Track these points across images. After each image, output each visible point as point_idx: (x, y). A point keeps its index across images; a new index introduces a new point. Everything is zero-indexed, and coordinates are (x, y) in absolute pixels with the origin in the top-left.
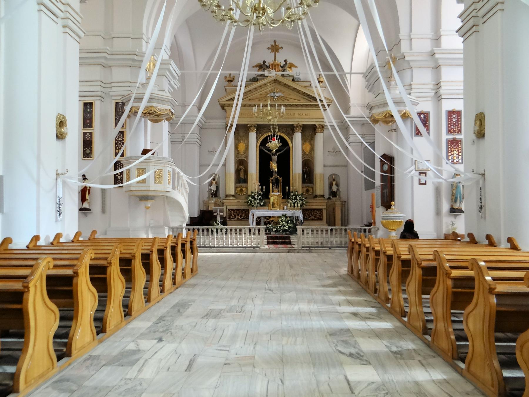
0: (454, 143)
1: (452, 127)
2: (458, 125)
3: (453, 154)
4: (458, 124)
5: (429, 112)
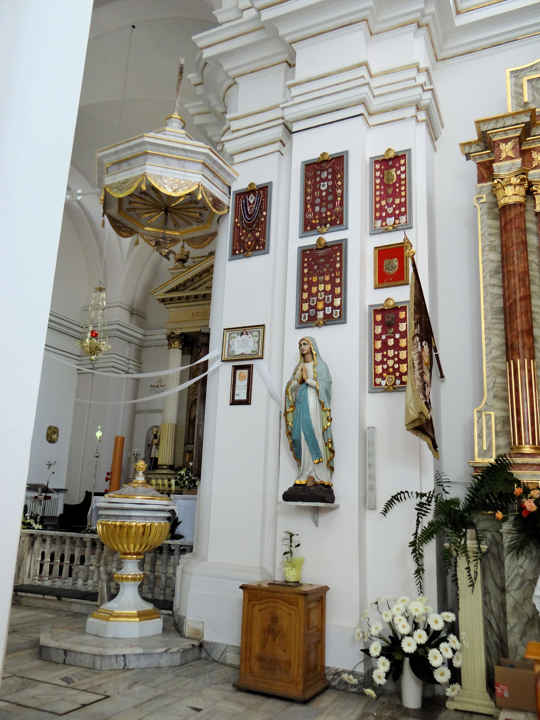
1: (317, 209)
3: (316, 295)
4: (336, 197)
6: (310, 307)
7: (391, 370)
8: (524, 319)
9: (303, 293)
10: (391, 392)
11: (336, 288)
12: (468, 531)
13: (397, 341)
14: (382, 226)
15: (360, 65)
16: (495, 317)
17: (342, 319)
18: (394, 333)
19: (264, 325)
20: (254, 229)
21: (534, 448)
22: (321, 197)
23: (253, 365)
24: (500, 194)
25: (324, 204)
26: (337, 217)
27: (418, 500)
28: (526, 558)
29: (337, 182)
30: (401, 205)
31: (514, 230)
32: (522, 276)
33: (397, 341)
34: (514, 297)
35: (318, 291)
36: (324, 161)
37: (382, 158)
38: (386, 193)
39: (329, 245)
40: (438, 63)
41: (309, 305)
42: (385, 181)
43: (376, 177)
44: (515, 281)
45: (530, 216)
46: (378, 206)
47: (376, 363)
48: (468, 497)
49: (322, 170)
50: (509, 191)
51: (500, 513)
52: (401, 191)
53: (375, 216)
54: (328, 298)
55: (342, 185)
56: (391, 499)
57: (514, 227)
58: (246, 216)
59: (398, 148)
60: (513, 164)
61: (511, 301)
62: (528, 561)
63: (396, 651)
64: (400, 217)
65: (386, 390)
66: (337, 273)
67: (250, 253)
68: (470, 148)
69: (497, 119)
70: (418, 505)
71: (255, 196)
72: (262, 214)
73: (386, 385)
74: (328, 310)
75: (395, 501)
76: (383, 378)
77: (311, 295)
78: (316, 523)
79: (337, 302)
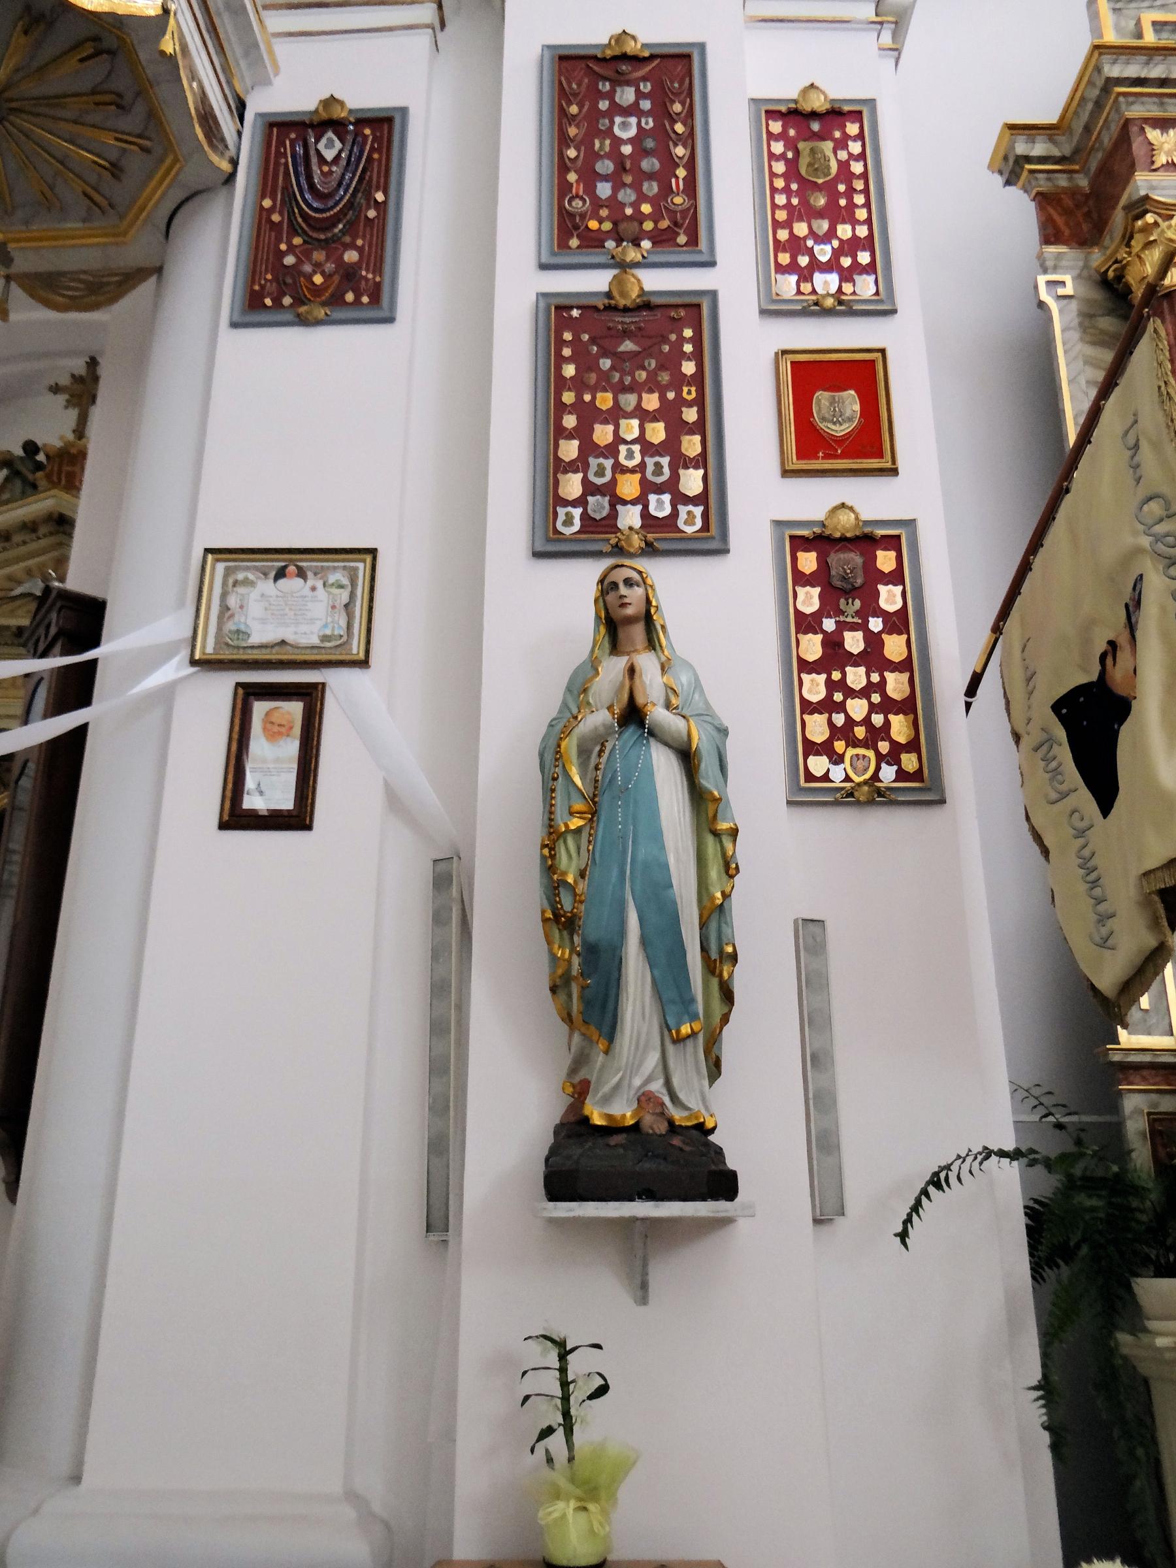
0: (626, 334)
1: (604, 190)
2: (664, 177)
3: (611, 450)
4: (671, 164)
5: (404, 111)
6: (589, 488)
7: (860, 732)
9: (562, 442)
13: (874, 642)
19: (373, 552)
20: (336, 239)
23: (324, 684)
29: (673, 121)
30: (852, 246)
33: (874, 642)
35: (618, 440)
36: (624, 57)
38: (804, 202)
41: (585, 482)
42: (803, 172)
46: (783, 235)
49: (620, 81)
52: (852, 206)
54: (658, 466)
55: (691, 133)
58: (308, 196)
64: (856, 277)
65: (848, 798)
66: (685, 389)
67: (321, 313)
68: (1030, 145)
71: (342, 140)
72: (369, 197)
73: (848, 779)
74: (661, 505)
76: (837, 759)
77: (589, 448)
78: (642, 1292)
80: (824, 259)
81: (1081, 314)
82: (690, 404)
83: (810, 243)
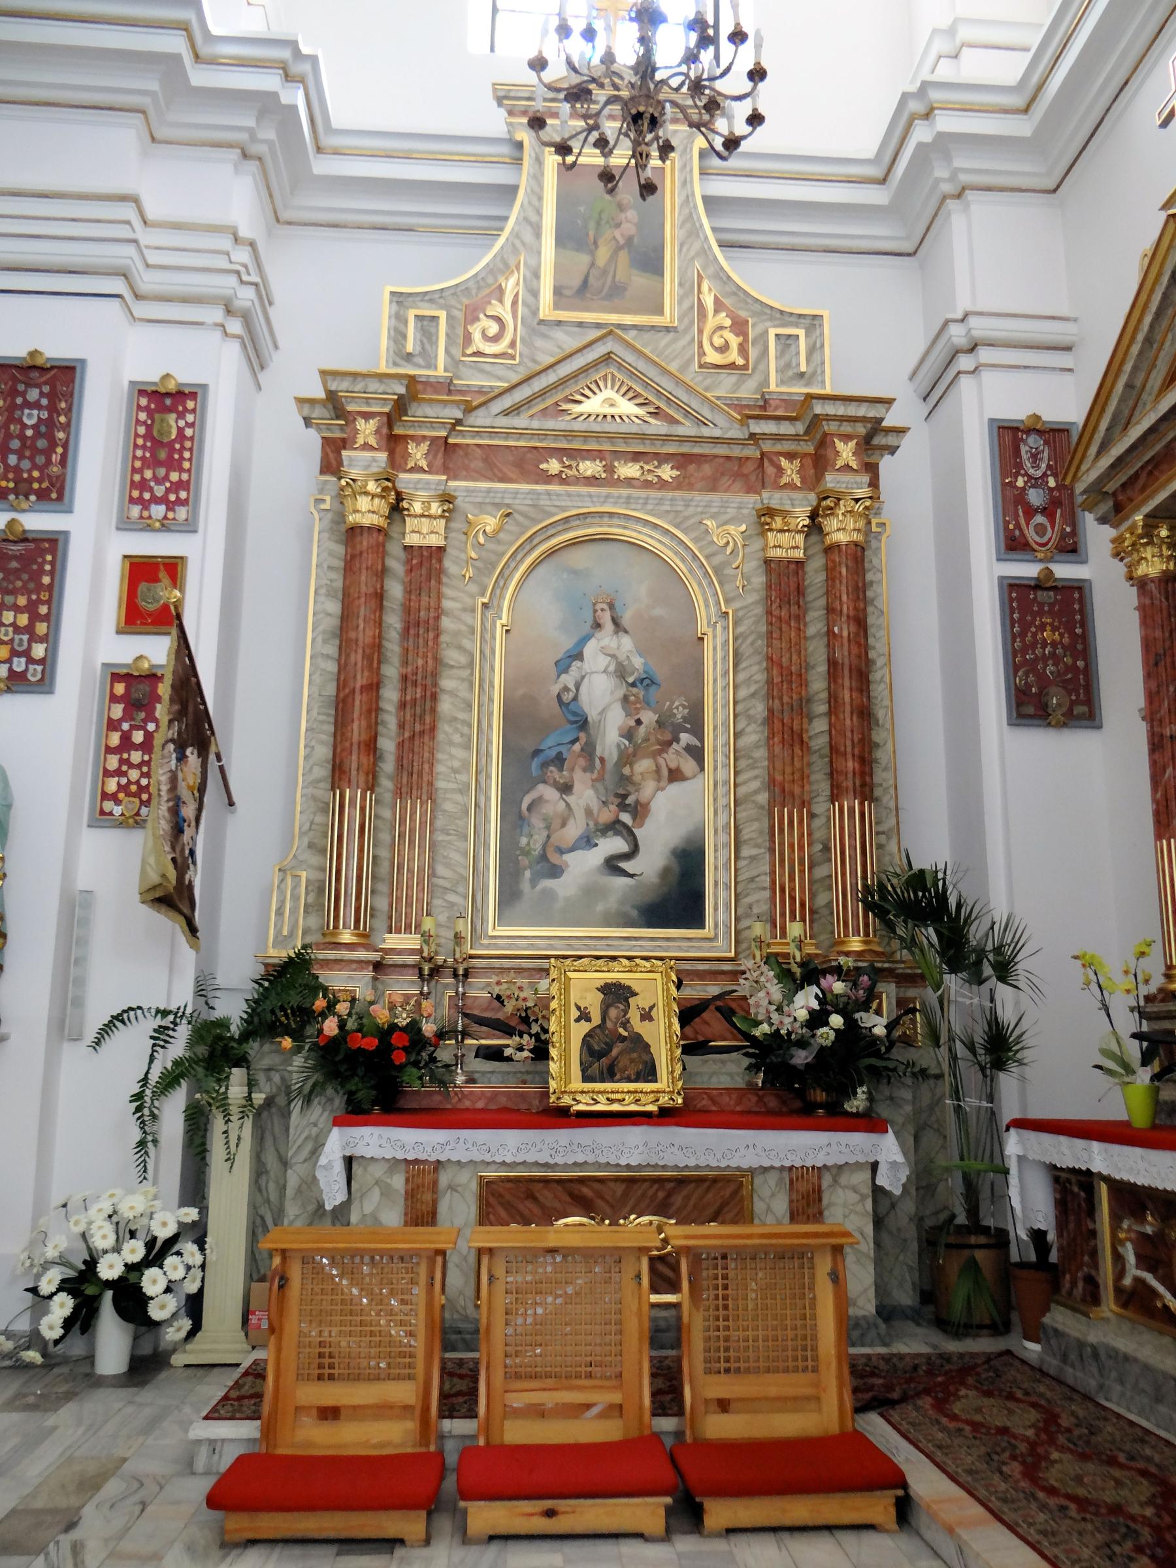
1: (12, 460)
8: (364, 723)
10: (128, 827)
11: (38, 624)
12: (234, 1070)
14: (141, 517)
15: (123, 198)
16: (323, 710)
17: (45, 685)
18: (145, 721)
21: (358, 935)
22: (22, 437)
24: (349, 502)
25: (27, 453)
26: (53, 485)
27: (159, 1021)
28: (324, 1110)
29: (59, 415)
31: (364, 571)
32: (368, 651)
34: (352, 685)
37: (154, 388)
38: (153, 455)
39: (30, 536)
40: (278, 226)
43: (138, 422)
44: (357, 657)
45: (394, 549)
46: (137, 478)
47: (107, 773)
48: (245, 1016)
49: (29, 385)
50: (363, 503)
51: (290, 1040)
52: (182, 458)
53: (130, 496)
56: (110, 1022)
57: (364, 566)
59: (185, 376)
60: (374, 460)
61: (347, 691)
62: (326, 1114)
63: (88, 1281)
64: (177, 508)
65: (121, 823)
69: (355, 375)
70: (155, 1031)
73: (122, 814)
75: (118, 1024)
76: (118, 802)
79: (39, 651)
80: (159, 495)
81: (333, 521)
82: (43, 603)
83: (152, 484)
